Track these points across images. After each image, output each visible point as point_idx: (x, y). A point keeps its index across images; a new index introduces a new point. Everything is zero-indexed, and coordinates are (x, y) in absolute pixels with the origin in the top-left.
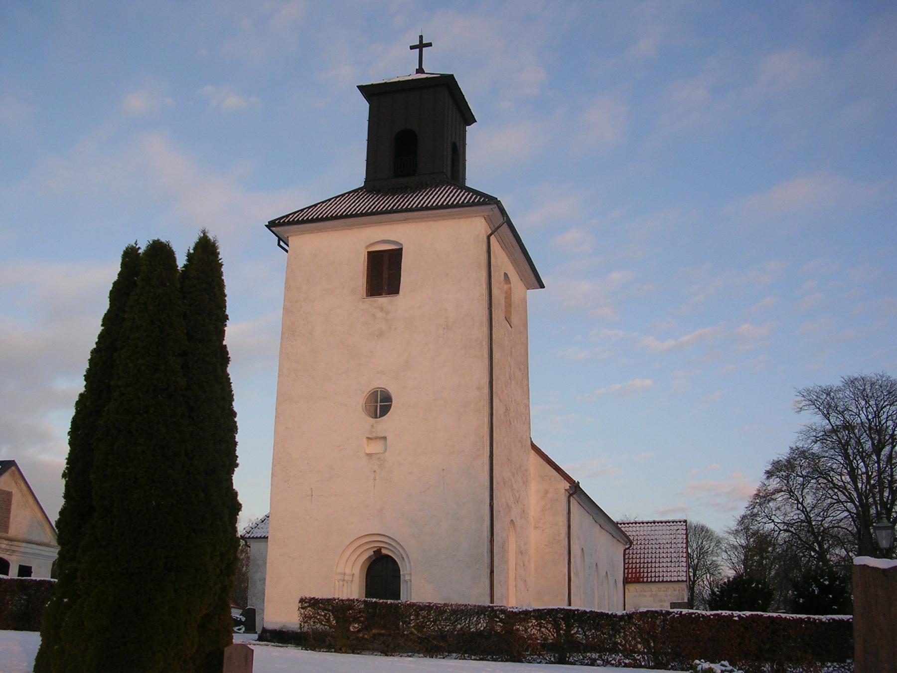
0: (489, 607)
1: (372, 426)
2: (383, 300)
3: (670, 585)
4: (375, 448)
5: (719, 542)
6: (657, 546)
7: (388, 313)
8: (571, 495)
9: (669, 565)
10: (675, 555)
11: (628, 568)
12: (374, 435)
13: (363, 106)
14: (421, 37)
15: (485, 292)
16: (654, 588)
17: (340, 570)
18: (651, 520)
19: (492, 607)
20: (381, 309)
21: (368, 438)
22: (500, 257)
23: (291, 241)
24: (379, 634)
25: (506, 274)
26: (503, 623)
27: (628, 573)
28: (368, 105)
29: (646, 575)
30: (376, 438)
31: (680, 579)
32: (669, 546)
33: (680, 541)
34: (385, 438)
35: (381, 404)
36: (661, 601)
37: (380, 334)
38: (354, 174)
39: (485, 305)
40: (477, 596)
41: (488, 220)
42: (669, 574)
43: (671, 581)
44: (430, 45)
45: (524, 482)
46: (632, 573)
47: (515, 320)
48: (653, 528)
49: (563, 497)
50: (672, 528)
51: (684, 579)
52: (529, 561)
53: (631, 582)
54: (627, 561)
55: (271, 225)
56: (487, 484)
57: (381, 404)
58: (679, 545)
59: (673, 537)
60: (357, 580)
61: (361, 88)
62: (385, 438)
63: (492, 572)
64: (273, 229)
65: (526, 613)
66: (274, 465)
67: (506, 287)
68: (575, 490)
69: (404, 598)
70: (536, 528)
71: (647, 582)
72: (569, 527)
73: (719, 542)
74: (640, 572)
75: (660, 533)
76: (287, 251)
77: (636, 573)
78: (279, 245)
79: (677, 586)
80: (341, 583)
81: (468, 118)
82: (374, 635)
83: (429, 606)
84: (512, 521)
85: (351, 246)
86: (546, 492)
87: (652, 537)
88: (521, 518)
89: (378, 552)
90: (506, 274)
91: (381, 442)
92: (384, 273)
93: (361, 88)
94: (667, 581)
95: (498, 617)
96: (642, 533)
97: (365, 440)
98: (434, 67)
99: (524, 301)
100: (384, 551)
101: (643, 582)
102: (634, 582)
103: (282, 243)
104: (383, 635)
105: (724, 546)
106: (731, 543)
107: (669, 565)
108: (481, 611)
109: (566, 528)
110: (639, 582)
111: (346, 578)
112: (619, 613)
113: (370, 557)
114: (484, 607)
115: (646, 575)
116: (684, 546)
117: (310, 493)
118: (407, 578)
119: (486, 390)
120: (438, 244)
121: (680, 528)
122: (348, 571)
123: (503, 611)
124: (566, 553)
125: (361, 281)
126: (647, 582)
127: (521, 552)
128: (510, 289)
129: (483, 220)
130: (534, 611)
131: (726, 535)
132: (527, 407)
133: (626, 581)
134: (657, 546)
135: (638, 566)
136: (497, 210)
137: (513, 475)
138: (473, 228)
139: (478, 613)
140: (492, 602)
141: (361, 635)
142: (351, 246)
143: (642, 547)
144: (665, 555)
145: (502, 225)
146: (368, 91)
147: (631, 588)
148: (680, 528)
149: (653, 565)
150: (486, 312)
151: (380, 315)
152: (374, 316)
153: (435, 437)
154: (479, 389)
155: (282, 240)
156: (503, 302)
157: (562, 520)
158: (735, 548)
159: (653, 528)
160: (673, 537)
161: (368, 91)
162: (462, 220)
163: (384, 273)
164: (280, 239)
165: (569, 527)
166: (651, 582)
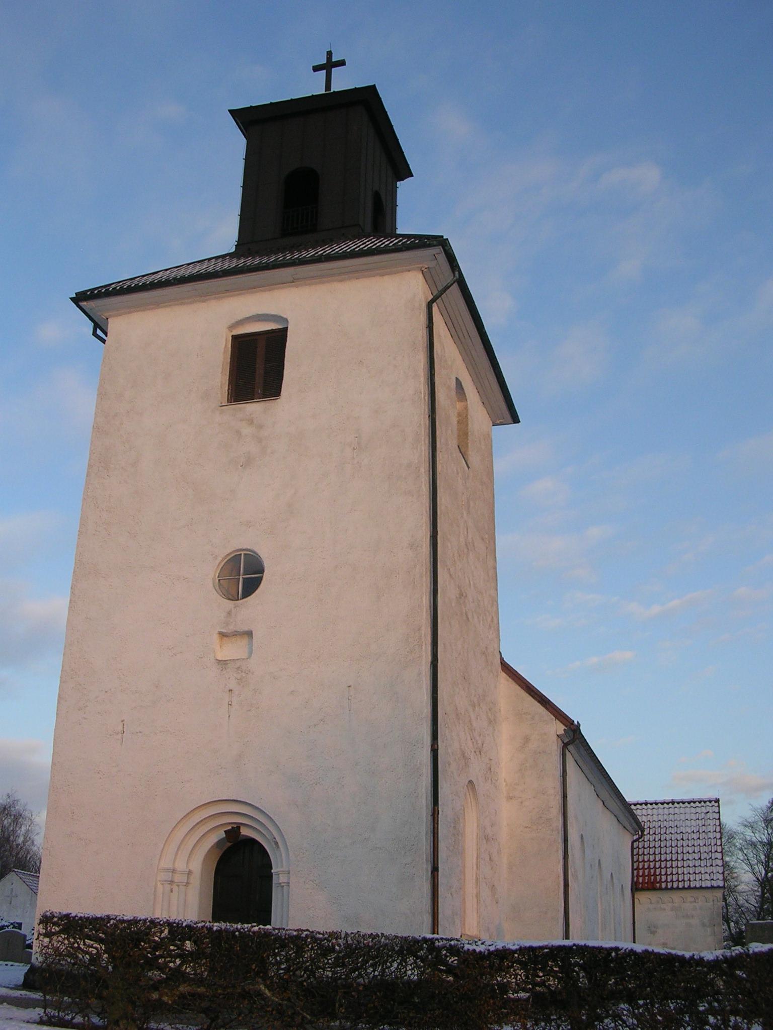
0: (425, 940)
1: (229, 613)
2: (253, 408)
3: (700, 894)
4: (232, 650)
5: (731, 837)
6: (679, 837)
7: (261, 427)
8: (565, 746)
9: (697, 863)
10: (706, 849)
11: (638, 869)
12: (232, 628)
13: (235, 145)
14: (330, 54)
15: (424, 389)
16: (676, 896)
17: (166, 863)
18: (668, 798)
19: (432, 941)
20: (251, 422)
21: (223, 635)
22: (447, 348)
23: (115, 325)
24: (193, 995)
25: (458, 383)
26: (455, 976)
27: (638, 876)
28: (243, 141)
29: (664, 878)
30: (236, 634)
31: (715, 884)
32: (695, 836)
33: (711, 828)
34: (249, 634)
35: (245, 575)
36: (687, 916)
37: (248, 462)
38: (222, 234)
39: (424, 408)
40: (403, 919)
41: (429, 276)
42: (698, 877)
43: (701, 888)
44: (342, 63)
45: (490, 722)
46: (643, 875)
47: (474, 458)
48: (671, 811)
49: (555, 748)
50: (698, 810)
51: (721, 884)
52: (499, 852)
53: (642, 889)
54: (635, 858)
55: (79, 299)
56: (427, 710)
57: (245, 575)
58: (711, 835)
59: (700, 823)
60: (196, 881)
61: (232, 112)
62: (249, 634)
63: (435, 869)
64: (83, 304)
65: (503, 954)
66: (63, 681)
67: (459, 405)
68: (573, 737)
69: (277, 921)
70: (510, 798)
71: (666, 888)
72: (565, 797)
73: (731, 837)
74: (655, 874)
75: (683, 817)
76: (104, 341)
77: (649, 875)
78: (95, 334)
79: (709, 894)
80: (168, 887)
81: (402, 171)
82: (182, 996)
83: (298, 937)
84: (470, 782)
85: (206, 327)
86: (527, 740)
87: (671, 824)
88: (486, 779)
89: (233, 833)
90: (458, 383)
91: (245, 641)
92: (257, 367)
93: (232, 112)
94: (695, 888)
95: (445, 964)
96: (655, 818)
97: (216, 637)
98: (342, 81)
99: (488, 438)
100: (244, 832)
101: (660, 889)
102: (648, 889)
103: (99, 332)
104: (201, 996)
105: (738, 842)
106: (748, 838)
107: (697, 863)
108: (409, 947)
109: (559, 798)
110: (654, 889)
111: (178, 878)
112: (709, 956)
113: (219, 844)
114: (416, 941)
115: (664, 878)
116: (718, 835)
117: (120, 728)
118: (283, 879)
119: (426, 549)
120: (348, 320)
121: (710, 810)
122: (181, 865)
123: (454, 950)
124: (560, 840)
125: (218, 376)
126: (666, 888)
127: (486, 838)
128: (466, 408)
129: (420, 276)
130: (522, 950)
131: (740, 829)
132: (494, 601)
133: (636, 888)
134: (679, 837)
135: (652, 865)
136: (442, 258)
137: (474, 706)
138: (400, 291)
139: (400, 953)
140: (434, 930)
141: (155, 996)
142: (206, 327)
143: (657, 837)
144: (690, 850)
145: (452, 287)
146: (247, 118)
147: (643, 897)
148: (710, 810)
149: (674, 864)
150: (426, 422)
151: (247, 430)
152: (238, 433)
153: (335, 631)
154: (411, 546)
155: (99, 328)
156: (454, 420)
157: (553, 785)
158: (753, 844)
159: (671, 811)
160: (700, 823)
161: (247, 118)
162: (386, 278)
163: (257, 367)
164: (96, 326)
165: (565, 797)
166: (672, 888)
